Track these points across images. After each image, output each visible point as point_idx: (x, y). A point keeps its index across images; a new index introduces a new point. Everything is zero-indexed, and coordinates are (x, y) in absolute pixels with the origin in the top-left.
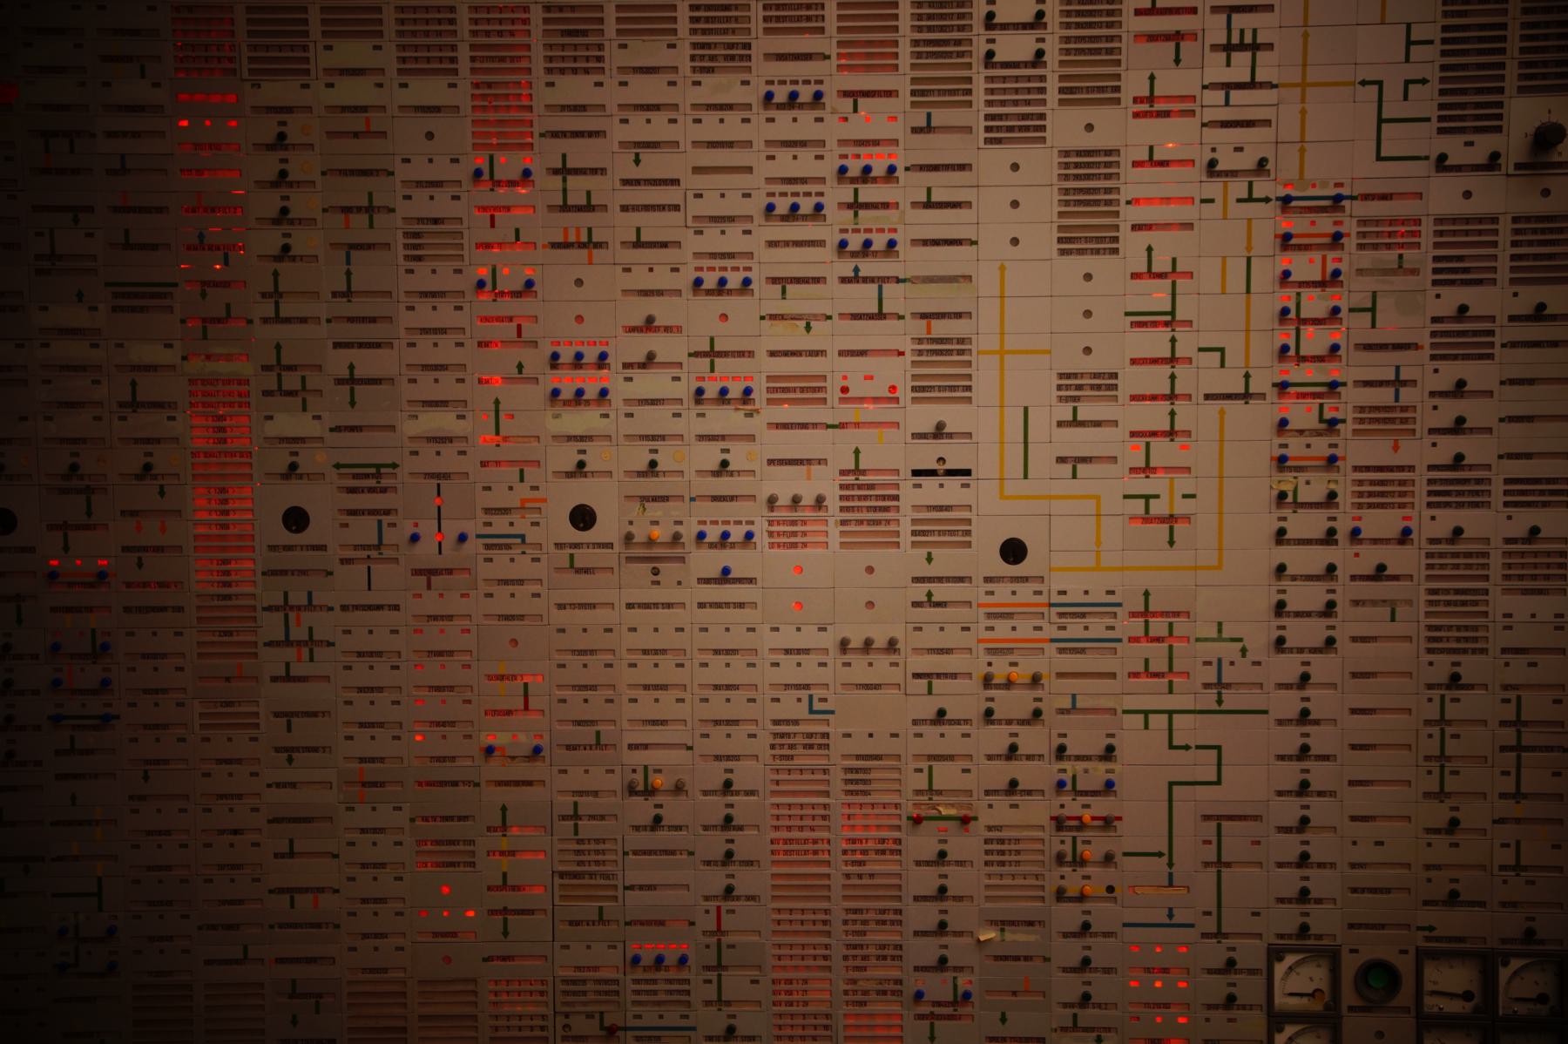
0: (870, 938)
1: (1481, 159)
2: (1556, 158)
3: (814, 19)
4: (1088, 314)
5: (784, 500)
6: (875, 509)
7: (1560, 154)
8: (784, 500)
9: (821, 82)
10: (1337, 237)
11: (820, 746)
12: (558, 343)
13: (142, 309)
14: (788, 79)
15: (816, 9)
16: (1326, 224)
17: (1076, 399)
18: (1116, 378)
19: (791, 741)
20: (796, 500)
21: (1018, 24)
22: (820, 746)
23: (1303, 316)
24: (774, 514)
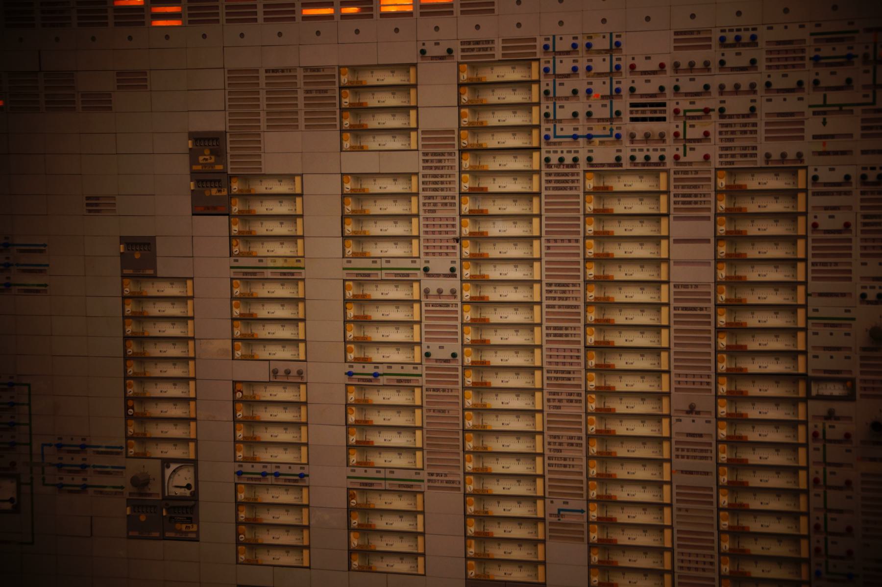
0: (735, 144)
1: (841, 82)
2: (151, 492)
3: (699, 203)
4: (648, 19)
5: (433, 292)
6: (689, 187)
7: (149, 489)
8: (433, 292)
9: (754, 29)
10: (849, 57)
11: (751, 132)
12: (591, 37)
13: (825, 371)
14: (750, 27)
15: (701, 197)
16: (841, 50)
17: (825, 113)
18: (756, 149)
19: (733, 152)
20: (440, 291)
21: (739, 115)
22: (751, 132)
23: (557, 50)
24: (428, 300)
